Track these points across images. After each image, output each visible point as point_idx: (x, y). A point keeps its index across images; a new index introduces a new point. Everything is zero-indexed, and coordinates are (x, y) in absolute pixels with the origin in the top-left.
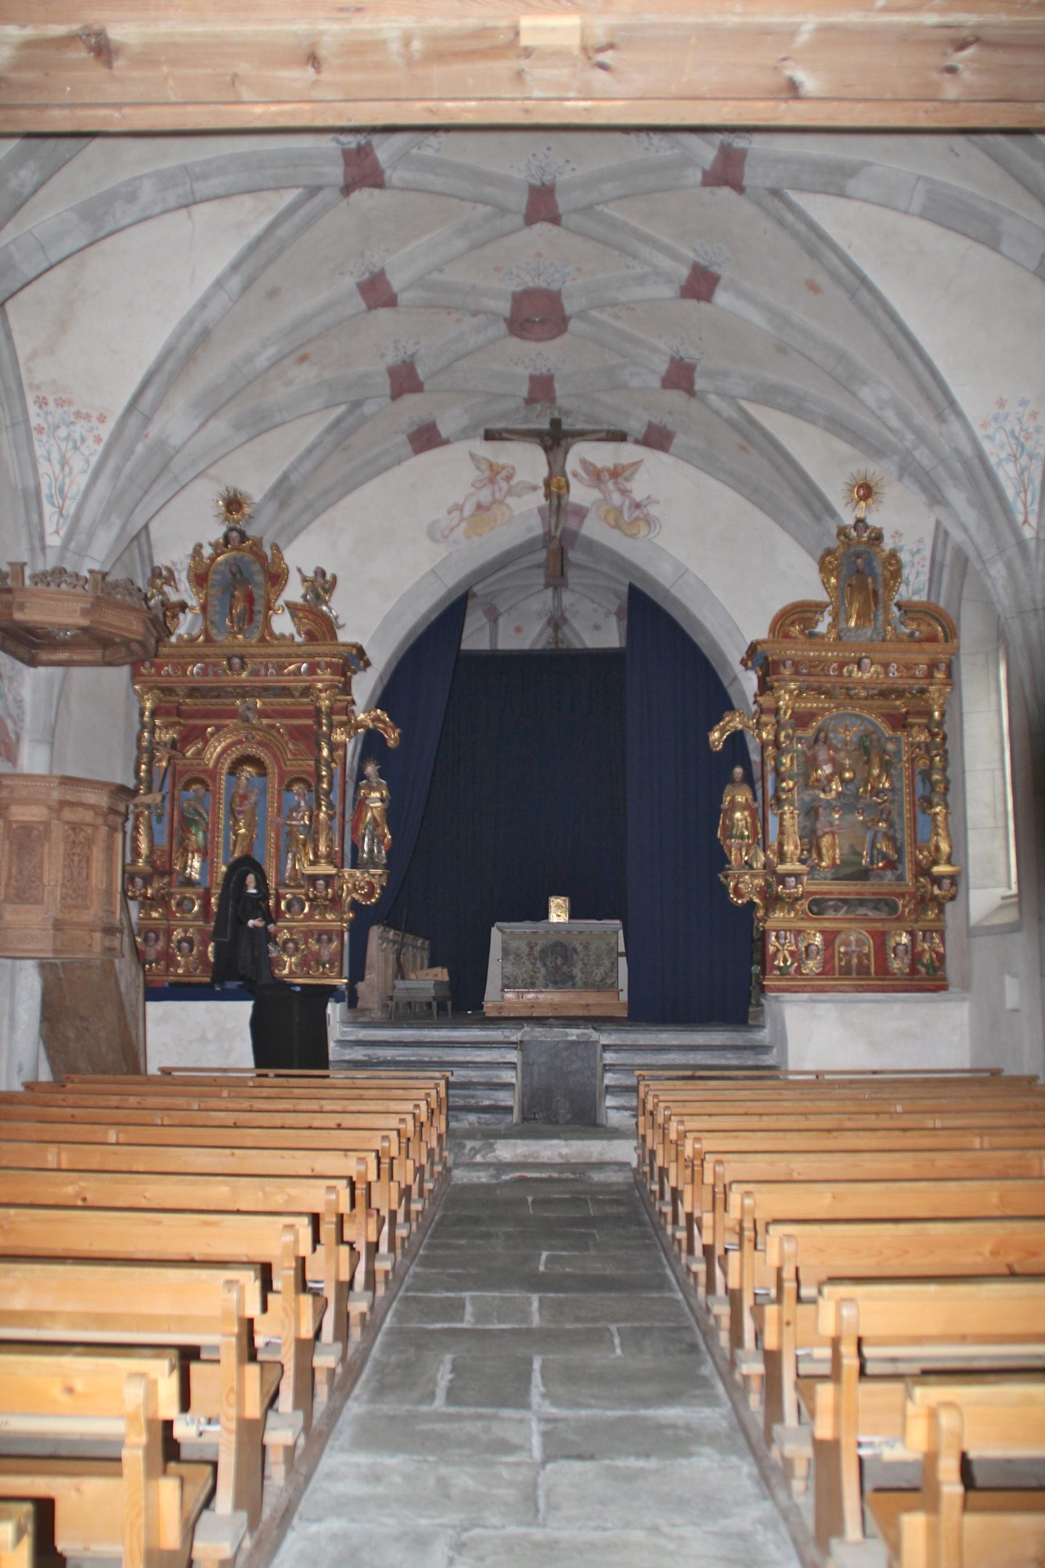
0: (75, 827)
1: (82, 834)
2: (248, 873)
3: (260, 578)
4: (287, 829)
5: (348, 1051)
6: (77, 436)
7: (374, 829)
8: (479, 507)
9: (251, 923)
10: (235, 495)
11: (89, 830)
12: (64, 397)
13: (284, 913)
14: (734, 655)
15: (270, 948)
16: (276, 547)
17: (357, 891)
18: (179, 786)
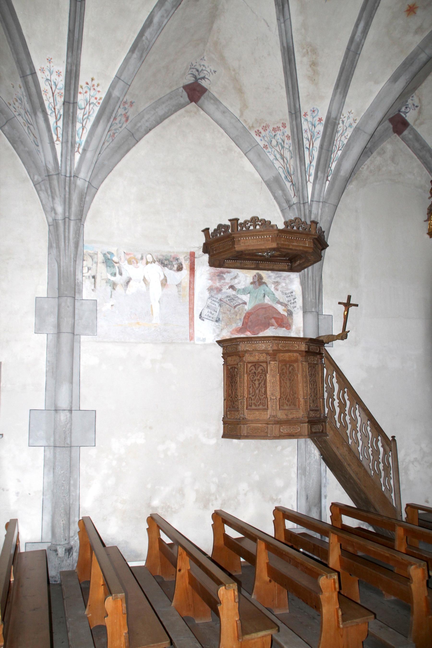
0: (284, 362)
1: (261, 368)
6: (280, 141)
11: (264, 365)
12: (265, 125)
14: (291, 139)
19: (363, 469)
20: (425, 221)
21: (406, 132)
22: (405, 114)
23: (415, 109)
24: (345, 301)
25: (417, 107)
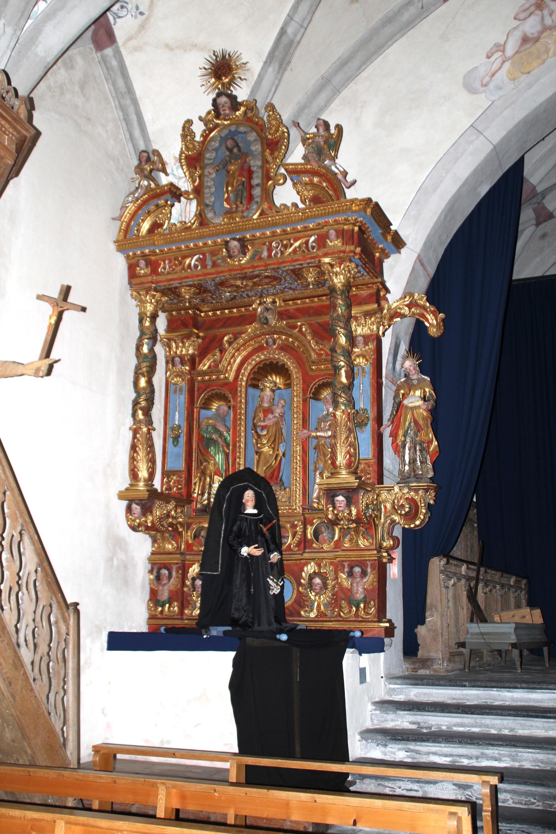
2: (245, 489)
3: (256, 148)
4: (314, 442)
5: (391, 716)
7: (416, 434)
8: (525, 40)
9: (245, 551)
10: (224, 57)
13: (311, 542)
15: (271, 582)
16: (271, 107)
17: (396, 511)
18: (198, 404)
19: (22, 672)
20: (113, 219)
21: (109, 51)
22: (114, 19)
23: (136, 17)
24: (55, 293)
25: (141, 14)
